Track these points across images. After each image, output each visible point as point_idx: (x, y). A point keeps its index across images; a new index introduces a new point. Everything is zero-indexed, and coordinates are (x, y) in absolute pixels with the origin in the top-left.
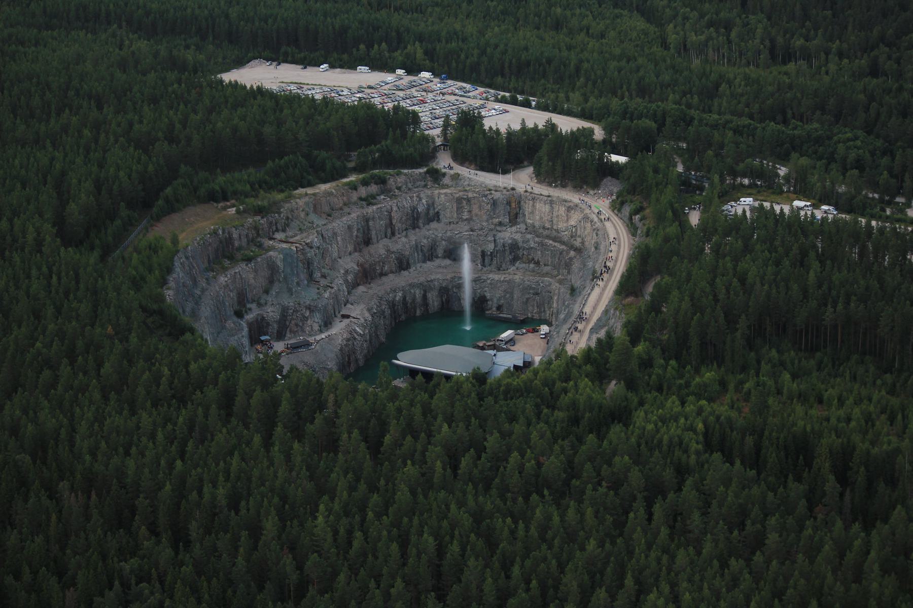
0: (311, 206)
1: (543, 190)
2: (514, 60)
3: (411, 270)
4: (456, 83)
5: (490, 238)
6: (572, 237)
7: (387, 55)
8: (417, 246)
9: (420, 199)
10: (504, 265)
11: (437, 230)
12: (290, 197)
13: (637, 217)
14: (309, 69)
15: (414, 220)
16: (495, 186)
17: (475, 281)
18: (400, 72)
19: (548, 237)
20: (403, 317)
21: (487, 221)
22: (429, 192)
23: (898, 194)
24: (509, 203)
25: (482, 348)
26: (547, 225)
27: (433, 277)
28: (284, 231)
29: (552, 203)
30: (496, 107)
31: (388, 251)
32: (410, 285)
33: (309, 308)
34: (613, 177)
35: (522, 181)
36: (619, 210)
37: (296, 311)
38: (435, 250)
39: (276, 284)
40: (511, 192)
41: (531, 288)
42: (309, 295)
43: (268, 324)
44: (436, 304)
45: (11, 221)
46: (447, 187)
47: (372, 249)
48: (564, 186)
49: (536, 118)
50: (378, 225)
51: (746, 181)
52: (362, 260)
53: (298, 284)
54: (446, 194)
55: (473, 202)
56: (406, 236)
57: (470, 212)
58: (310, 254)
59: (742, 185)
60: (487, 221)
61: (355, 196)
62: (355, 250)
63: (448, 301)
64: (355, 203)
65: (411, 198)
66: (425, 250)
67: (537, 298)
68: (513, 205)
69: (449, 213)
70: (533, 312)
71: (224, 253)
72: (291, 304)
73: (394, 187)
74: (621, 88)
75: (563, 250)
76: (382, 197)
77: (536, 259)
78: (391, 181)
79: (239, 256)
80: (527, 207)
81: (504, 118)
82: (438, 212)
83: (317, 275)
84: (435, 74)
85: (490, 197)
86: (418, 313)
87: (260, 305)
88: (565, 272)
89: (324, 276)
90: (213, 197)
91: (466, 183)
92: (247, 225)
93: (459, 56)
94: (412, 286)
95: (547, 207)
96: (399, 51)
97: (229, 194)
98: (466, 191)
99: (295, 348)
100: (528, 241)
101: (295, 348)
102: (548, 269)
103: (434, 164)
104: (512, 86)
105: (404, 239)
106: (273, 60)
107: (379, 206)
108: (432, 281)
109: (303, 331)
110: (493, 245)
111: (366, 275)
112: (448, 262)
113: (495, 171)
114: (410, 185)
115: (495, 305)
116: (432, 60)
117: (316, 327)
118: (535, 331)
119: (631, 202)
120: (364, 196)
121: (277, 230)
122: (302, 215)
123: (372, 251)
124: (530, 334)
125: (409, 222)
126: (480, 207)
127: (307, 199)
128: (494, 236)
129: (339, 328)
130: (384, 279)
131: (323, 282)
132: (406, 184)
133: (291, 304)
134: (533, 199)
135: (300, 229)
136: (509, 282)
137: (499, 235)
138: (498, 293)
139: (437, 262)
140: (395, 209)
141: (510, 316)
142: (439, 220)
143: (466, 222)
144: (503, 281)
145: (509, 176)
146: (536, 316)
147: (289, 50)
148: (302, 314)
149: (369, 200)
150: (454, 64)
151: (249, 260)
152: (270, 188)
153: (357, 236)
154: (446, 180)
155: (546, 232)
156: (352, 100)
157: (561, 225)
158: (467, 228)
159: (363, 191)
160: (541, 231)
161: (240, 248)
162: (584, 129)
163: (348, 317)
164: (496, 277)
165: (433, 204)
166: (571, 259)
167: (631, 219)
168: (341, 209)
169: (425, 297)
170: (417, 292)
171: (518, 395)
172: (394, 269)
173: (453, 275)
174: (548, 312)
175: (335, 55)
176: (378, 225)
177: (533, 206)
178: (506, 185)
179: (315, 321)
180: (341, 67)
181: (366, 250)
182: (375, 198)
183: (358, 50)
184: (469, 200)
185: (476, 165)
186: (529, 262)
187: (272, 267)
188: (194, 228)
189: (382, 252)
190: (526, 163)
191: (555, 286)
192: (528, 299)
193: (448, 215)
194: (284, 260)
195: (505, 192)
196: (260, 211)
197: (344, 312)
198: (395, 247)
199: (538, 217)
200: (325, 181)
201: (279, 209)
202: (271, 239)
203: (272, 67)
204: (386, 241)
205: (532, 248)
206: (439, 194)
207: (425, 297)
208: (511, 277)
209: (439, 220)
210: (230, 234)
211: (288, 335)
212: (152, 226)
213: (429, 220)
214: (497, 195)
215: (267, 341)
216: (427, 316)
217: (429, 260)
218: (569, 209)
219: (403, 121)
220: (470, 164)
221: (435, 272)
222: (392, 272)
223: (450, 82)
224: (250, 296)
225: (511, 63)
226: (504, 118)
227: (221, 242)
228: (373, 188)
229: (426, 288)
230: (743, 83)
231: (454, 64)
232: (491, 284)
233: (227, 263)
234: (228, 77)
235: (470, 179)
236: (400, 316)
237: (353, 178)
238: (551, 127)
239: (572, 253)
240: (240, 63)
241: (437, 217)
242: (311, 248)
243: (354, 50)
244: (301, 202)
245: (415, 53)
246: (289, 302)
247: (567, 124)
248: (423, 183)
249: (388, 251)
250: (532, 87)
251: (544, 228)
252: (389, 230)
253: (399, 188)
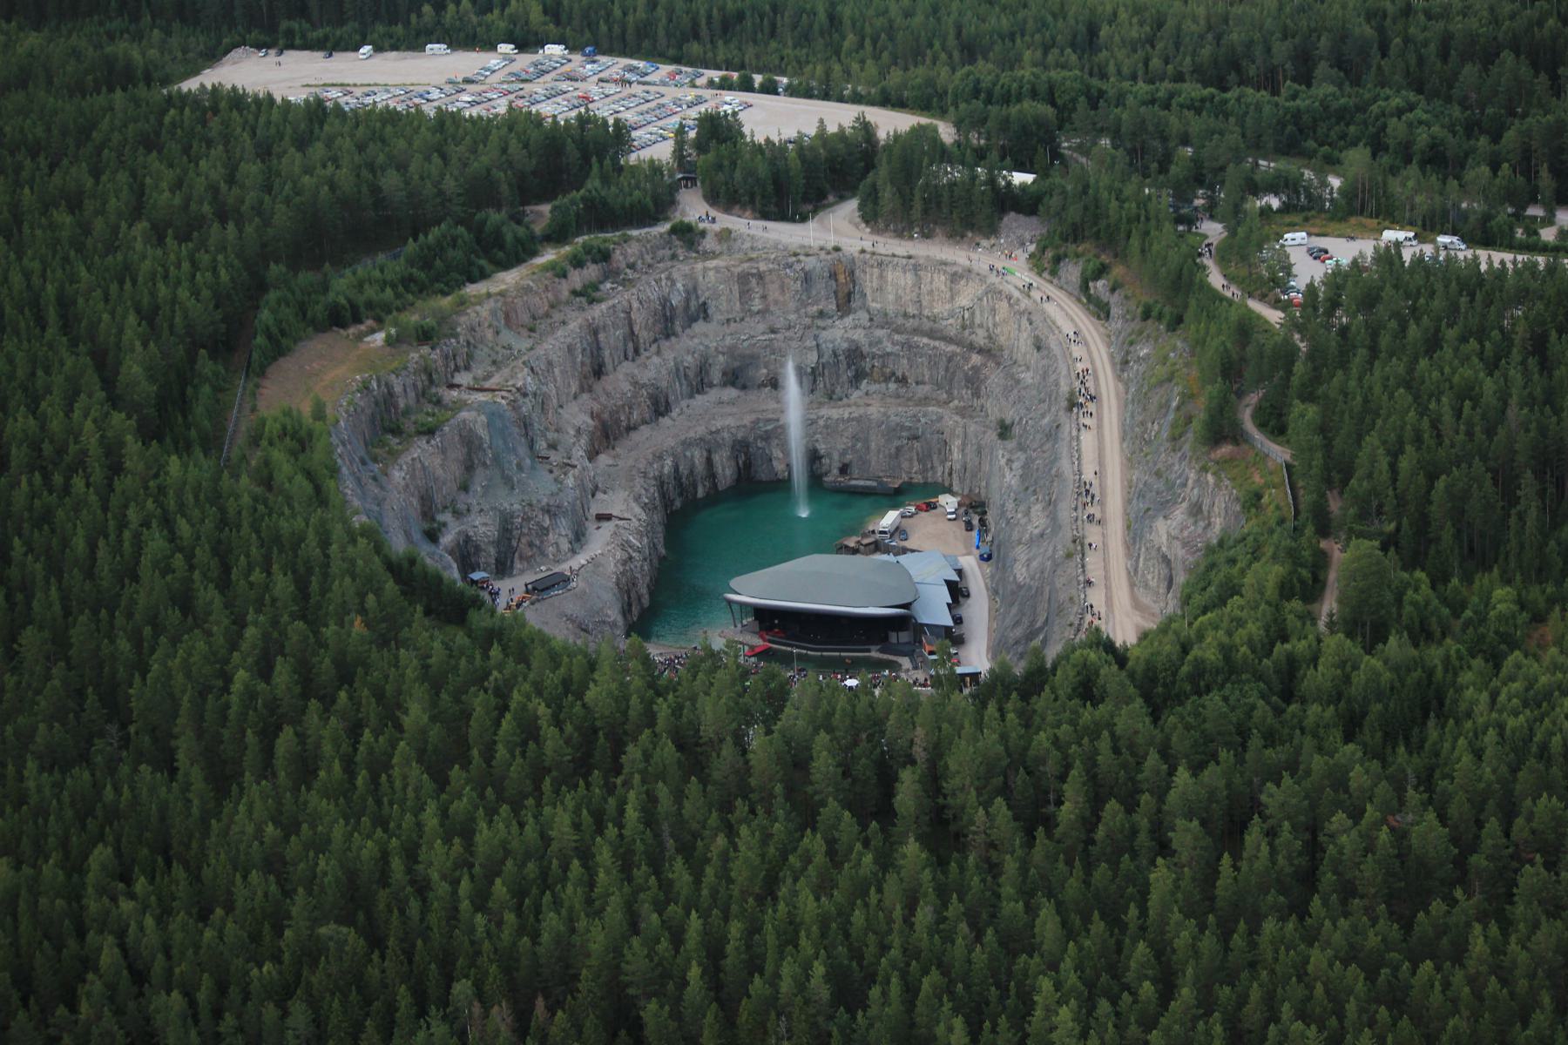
0: (501, 315)
1: (890, 246)
2: (715, 11)
3: (674, 414)
4: (617, 59)
5: (810, 343)
6: (964, 327)
7: (474, 19)
8: (678, 370)
9: (673, 283)
10: (838, 390)
11: (706, 336)
12: (463, 302)
13: (1100, 283)
14: (337, 56)
15: (668, 322)
16: (803, 247)
17: (810, 423)
18: (506, 48)
19: (916, 331)
20: (678, 504)
21: (797, 311)
22: (686, 269)
23: (1533, 200)
24: (833, 275)
25: (855, 551)
26: (911, 310)
27: (719, 424)
28: (467, 368)
29: (916, 268)
30: (728, 99)
31: (635, 384)
32: (684, 443)
33: (547, 510)
34: (1019, 211)
35: (838, 229)
36: (1054, 273)
37: (527, 519)
38: (707, 373)
39: (479, 472)
40: (835, 255)
41: (903, 428)
42: (541, 486)
43: (478, 548)
44: (728, 472)
45: (33, 410)
46: (714, 255)
47: (608, 382)
48: (927, 235)
49: (839, 117)
50: (612, 339)
51: (1275, 203)
52: (596, 407)
53: (520, 467)
54: (717, 269)
55: (768, 279)
56: (658, 353)
57: (764, 297)
58: (527, 406)
59: (1266, 212)
60: (797, 311)
61: (564, 288)
62: (582, 390)
63: (748, 465)
64: (567, 303)
65: (658, 281)
66: (691, 374)
67: (916, 444)
68: (842, 278)
69: (725, 303)
70: (911, 470)
71: (387, 425)
72: (516, 506)
73: (623, 265)
74: (931, 45)
75: (954, 354)
76: (609, 285)
77: (899, 374)
78: (617, 255)
79: (408, 426)
80: (869, 281)
81: (777, 119)
82: (704, 304)
83: (541, 445)
84: (572, 48)
85: (798, 267)
86: (701, 493)
87: (457, 514)
88: (967, 393)
89: (553, 446)
90: (340, 318)
91: (747, 245)
92: (412, 366)
93: (609, 14)
94: (687, 444)
95: (910, 277)
96: (496, 12)
97: (362, 309)
98: (751, 259)
99: (539, 589)
100: (880, 342)
101: (539, 589)
102: (924, 390)
103: (677, 214)
104: (721, 57)
105: (656, 360)
106: (269, 47)
107: (611, 303)
108: (718, 431)
109: (543, 554)
110: (815, 354)
111: (607, 434)
112: (731, 393)
113: (782, 216)
114: (648, 258)
115: (838, 465)
116: (558, 23)
117: (565, 546)
118: (931, 507)
119: (1077, 256)
120: (578, 287)
121: (457, 369)
122: (489, 334)
123: (609, 388)
124: (923, 514)
125: (659, 326)
126: (782, 288)
127: (491, 304)
128: (816, 337)
129: (600, 541)
130: (634, 436)
131: (555, 458)
132: (642, 257)
133: (516, 506)
134: (880, 264)
135: (494, 362)
136: (859, 420)
137: (824, 335)
138: (842, 443)
139: (713, 395)
140: (635, 305)
141: (874, 484)
142: (706, 318)
143: (758, 318)
144: (849, 419)
145: (811, 225)
146: (918, 479)
147: (295, 26)
148: (538, 524)
149: (589, 294)
150: (603, 28)
151: (430, 432)
152: (423, 290)
153: (583, 363)
154: (709, 243)
155: (910, 323)
156: (297, 96)
157: (940, 308)
158: (762, 327)
159: (577, 278)
160: (900, 321)
161: (407, 412)
162: (920, 126)
163: (608, 517)
164: (835, 413)
165: (695, 289)
166: (975, 369)
167: (1085, 287)
168: (547, 315)
169: (709, 462)
170: (697, 453)
171: (1220, 679)
172: (647, 416)
173: (754, 417)
174: (940, 470)
175: (380, 28)
176: (612, 339)
177: (881, 277)
178: (822, 243)
179: (560, 535)
180: (395, 48)
181: (598, 387)
182: (598, 289)
183: (420, 16)
184: (760, 276)
185: (754, 210)
186: (887, 380)
187: (470, 442)
188: (326, 380)
189: (626, 387)
190: (831, 198)
191: (951, 420)
192: (898, 449)
193: (724, 307)
194: (489, 425)
195: (823, 255)
196: (425, 336)
197: (595, 509)
198: (646, 376)
199: (891, 297)
200: (506, 266)
201: (453, 329)
202: (452, 386)
203: (268, 59)
204: (627, 367)
205: (888, 354)
206: (705, 270)
207: (709, 462)
208: (862, 411)
209: (706, 318)
210: (389, 386)
211: (518, 565)
212: (257, 386)
213: (692, 320)
214: (810, 263)
215: (484, 581)
216: (716, 497)
217: (698, 392)
218: (955, 278)
219: (599, 143)
220: (743, 207)
221: (719, 414)
222: (645, 422)
223: (603, 59)
224: (438, 499)
225: (709, 17)
226: (777, 119)
227: (377, 404)
228: (592, 271)
229: (709, 447)
230: (1135, 20)
231: (603, 28)
232: (827, 427)
233: (393, 441)
234: (190, 85)
235: (753, 238)
236: (672, 502)
237: (549, 256)
238: (866, 128)
239: (976, 359)
240: (213, 56)
241: (703, 312)
242: (525, 395)
243: (413, 18)
244: (484, 311)
245: (527, 14)
246: (511, 503)
247: (890, 123)
248: (668, 252)
249: (635, 384)
250: (758, 57)
251: (905, 315)
252: (630, 345)
253: (632, 266)
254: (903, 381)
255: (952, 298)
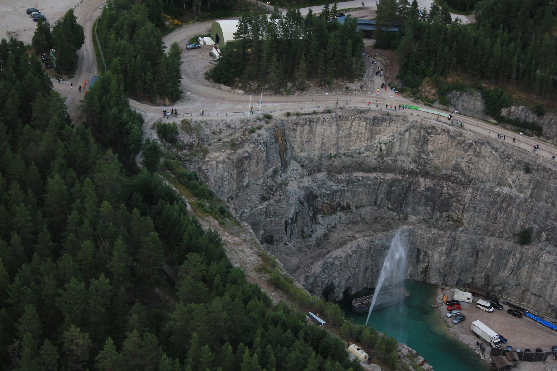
80: (297, 139)
177: (311, 131)
199: (317, 146)
220: (485, 103)
254: (346, 209)
255: (372, 137)
